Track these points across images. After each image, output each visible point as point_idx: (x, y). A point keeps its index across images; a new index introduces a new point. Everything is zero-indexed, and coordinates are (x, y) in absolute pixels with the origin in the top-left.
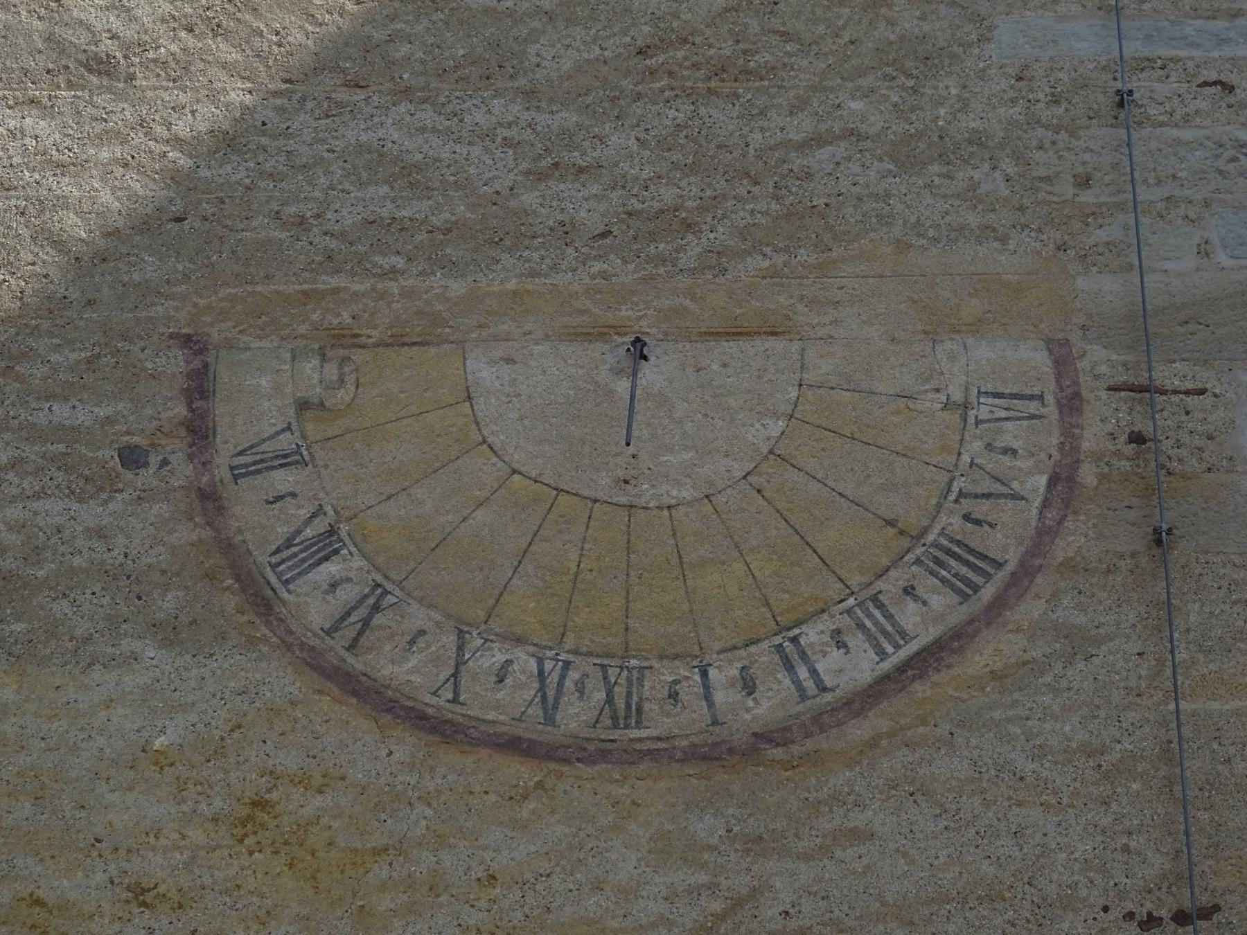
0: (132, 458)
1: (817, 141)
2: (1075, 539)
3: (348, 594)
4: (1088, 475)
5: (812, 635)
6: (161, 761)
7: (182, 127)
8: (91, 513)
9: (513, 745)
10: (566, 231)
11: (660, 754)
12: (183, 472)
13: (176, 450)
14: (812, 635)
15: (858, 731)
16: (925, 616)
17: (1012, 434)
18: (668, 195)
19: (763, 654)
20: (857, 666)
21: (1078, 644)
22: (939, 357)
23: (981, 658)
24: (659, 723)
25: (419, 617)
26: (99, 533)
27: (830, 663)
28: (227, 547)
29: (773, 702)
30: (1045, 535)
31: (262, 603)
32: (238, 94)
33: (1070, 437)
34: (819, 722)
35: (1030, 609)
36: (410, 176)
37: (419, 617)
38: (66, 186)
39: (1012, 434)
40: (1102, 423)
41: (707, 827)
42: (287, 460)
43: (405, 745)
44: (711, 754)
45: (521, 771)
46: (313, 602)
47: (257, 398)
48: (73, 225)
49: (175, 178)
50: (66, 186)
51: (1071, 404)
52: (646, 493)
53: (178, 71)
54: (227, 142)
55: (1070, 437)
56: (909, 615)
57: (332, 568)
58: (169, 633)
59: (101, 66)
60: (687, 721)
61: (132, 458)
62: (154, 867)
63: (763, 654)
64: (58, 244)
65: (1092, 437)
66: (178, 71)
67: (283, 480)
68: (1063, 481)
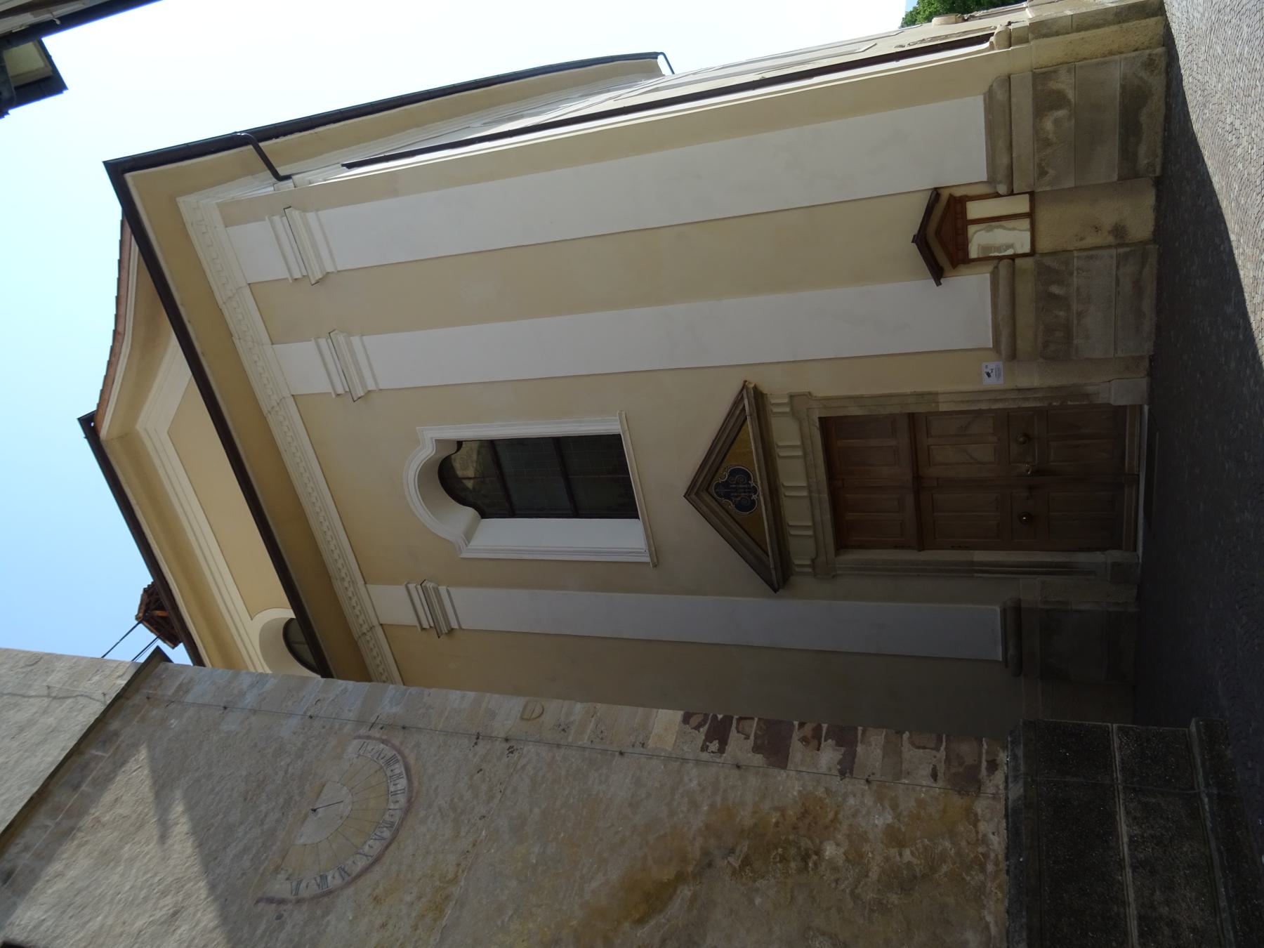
0: (279, 917)
1: (286, 772)
2: (396, 742)
3: (337, 875)
4: (384, 737)
5: (392, 789)
6: (355, 918)
7: (203, 897)
8: (288, 927)
9: (387, 847)
10: (278, 821)
11: (403, 820)
12: (290, 906)
13: (283, 907)
14: (392, 789)
15: (416, 784)
16: (399, 768)
17: (369, 748)
18: (281, 800)
19: (391, 798)
20: (403, 783)
21: (418, 745)
22: (162, 903)
23: (411, 760)
24: (396, 820)
25: (350, 862)
26: (294, 927)
27: (399, 787)
28: (312, 898)
29: (402, 800)
30: (393, 747)
31: (330, 892)
32: (202, 884)
33: (375, 739)
34: (411, 791)
35: (406, 752)
36: (246, 850)
37: (350, 862)
38: (202, 925)
39: (369, 748)
40: (376, 733)
41: (422, 814)
42: (299, 883)
43: (377, 868)
44: (407, 810)
45: (394, 846)
46: (334, 880)
47: (280, 887)
48: (212, 925)
49: (215, 900)
50: (202, 925)
51: (369, 737)
52: (346, 814)
53: (188, 896)
54: (212, 887)
55: (375, 739)
56: (397, 771)
57: (329, 878)
58: (326, 913)
59: (175, 914)
60: (398, 814)
61: (279, 917)
62: (378, 922)
63: (391, 798)
64: (215, 928)
65: (378, 735)
66: (188, 896)
67: (303, 885)
68: (383, 742)
